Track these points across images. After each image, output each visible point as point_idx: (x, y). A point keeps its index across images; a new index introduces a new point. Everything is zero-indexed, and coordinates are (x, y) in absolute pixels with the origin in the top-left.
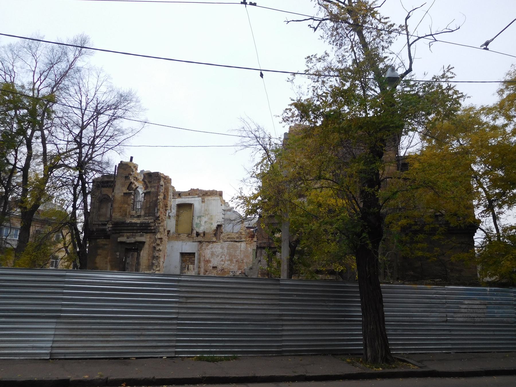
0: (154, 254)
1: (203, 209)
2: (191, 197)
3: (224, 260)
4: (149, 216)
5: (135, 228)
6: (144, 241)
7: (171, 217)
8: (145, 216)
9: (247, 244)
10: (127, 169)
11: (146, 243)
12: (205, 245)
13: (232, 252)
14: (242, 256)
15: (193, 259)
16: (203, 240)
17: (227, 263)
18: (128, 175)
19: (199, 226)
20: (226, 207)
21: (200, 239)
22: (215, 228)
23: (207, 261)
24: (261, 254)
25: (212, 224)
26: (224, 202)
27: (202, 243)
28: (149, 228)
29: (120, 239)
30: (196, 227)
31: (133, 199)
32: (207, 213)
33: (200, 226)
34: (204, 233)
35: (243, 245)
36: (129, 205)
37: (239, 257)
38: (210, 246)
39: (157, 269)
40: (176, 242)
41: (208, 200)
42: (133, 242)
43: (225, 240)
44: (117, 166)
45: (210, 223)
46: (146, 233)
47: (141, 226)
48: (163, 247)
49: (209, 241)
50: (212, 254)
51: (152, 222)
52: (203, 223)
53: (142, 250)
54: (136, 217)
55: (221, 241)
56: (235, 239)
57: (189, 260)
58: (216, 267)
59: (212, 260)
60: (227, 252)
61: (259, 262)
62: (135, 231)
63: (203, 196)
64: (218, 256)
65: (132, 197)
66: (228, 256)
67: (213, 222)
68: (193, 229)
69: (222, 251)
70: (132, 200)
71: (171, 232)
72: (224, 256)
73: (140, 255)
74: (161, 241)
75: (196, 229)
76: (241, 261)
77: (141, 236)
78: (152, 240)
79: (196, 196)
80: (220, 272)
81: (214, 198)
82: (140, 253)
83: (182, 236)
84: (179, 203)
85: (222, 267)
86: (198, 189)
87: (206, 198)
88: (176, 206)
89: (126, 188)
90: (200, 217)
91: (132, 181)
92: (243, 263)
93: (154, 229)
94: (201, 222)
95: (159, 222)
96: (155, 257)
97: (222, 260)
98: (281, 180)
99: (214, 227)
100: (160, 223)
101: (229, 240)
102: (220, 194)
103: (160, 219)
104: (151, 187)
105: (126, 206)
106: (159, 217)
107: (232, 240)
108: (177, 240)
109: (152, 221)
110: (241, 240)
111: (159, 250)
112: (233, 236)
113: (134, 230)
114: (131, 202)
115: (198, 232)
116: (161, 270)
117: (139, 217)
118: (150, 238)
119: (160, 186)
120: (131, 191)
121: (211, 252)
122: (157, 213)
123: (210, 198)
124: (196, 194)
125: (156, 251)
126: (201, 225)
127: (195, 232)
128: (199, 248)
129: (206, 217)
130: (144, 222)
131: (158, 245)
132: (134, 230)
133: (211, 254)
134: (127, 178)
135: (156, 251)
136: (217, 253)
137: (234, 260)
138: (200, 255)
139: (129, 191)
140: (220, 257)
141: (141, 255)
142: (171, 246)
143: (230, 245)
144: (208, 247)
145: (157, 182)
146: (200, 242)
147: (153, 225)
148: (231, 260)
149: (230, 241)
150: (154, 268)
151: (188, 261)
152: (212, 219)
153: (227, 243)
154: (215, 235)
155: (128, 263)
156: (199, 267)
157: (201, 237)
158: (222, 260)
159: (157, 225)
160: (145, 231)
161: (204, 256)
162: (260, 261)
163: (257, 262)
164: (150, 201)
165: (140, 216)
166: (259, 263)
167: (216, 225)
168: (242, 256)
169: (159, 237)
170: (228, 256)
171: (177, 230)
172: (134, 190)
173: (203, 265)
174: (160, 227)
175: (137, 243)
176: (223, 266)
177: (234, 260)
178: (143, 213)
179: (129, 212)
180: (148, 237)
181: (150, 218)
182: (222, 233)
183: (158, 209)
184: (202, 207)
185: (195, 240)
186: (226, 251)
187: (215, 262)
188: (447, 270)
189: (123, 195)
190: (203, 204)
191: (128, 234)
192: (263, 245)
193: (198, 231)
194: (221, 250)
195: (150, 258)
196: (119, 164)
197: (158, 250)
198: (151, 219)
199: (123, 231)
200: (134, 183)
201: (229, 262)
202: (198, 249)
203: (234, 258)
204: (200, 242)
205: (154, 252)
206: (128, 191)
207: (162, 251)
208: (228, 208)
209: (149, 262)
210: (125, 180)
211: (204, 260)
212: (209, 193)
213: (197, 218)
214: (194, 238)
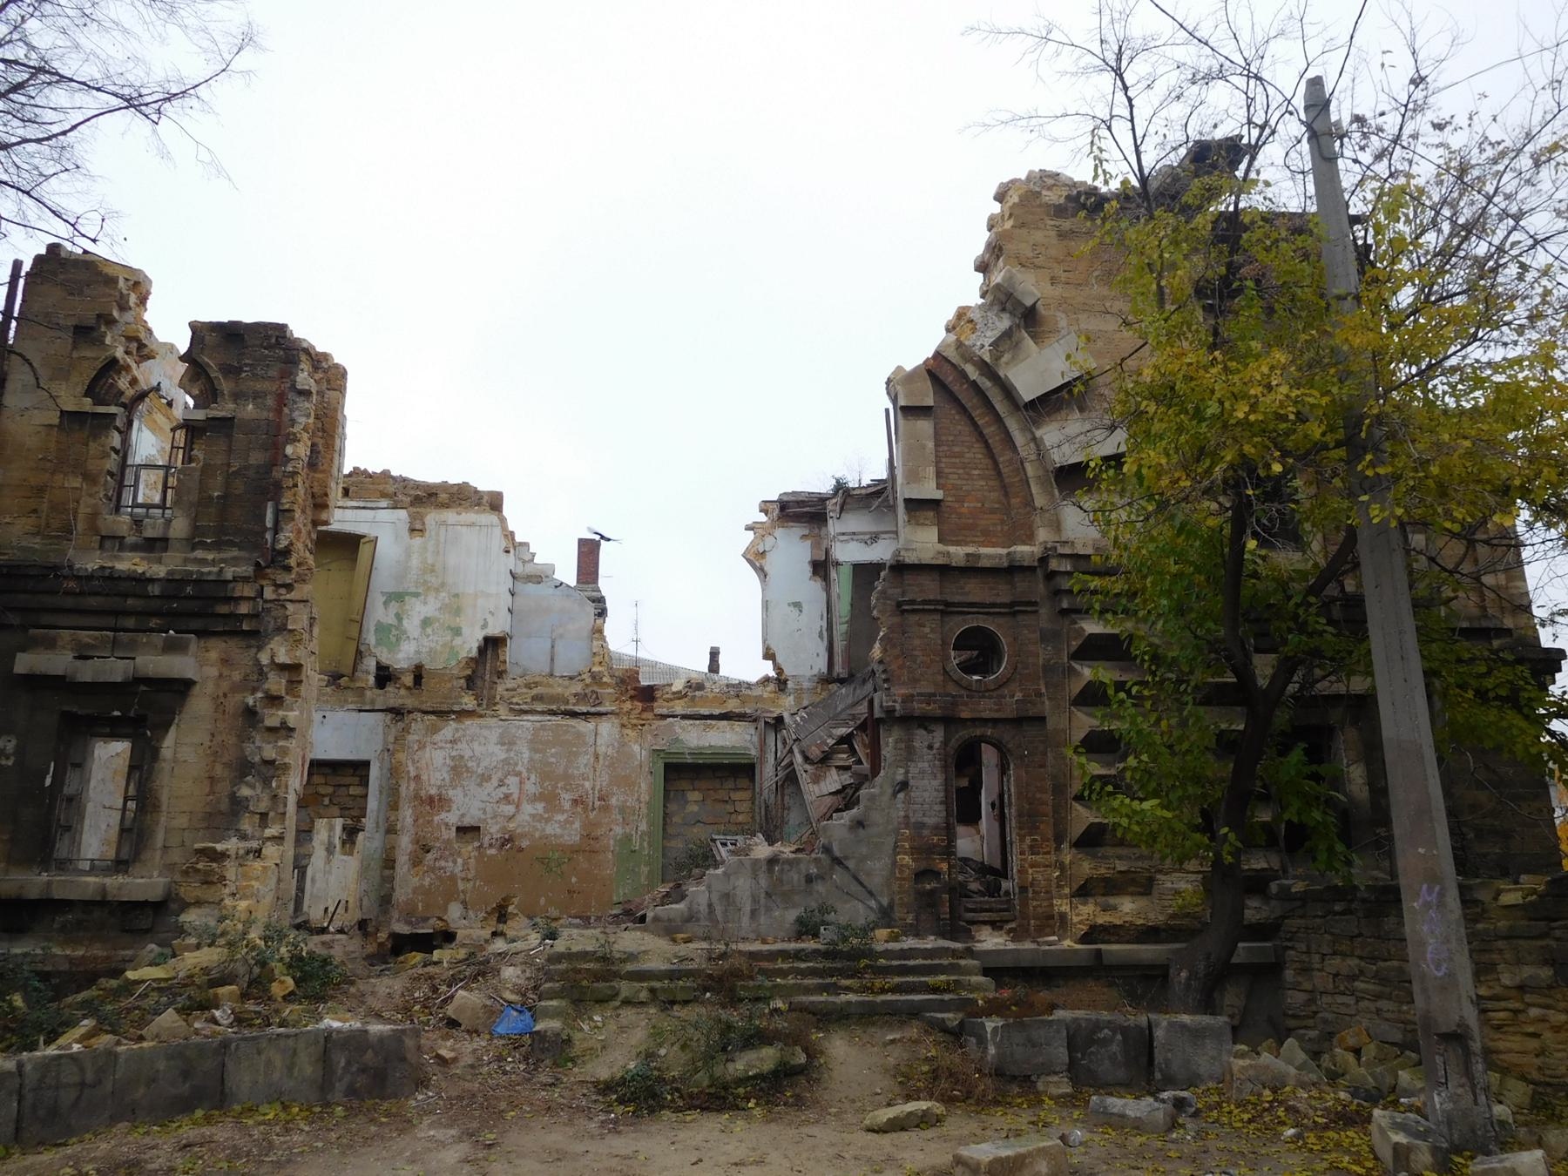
1: (415, 562)
3: (515, 796)
4: (218, 546)
5: (130, 601)
6: (190, 675)
8: (193, 542)
9: (623, 726)
10: (87, 291)
11: (197, 687)
12: (418, 725)
13: (553, 760)
14: (603, 779)
15: (353, 791)
16: (410, 702)
17: (528, 809)
18: (92, 322)
19: (393, 639)
20: (520, 564)
21: (394, 696)
22: (474, 653)
23: (431, 800)
24: (909, 754)
25: (457, 632)
26: (513, 546)
27: (408, 719)
28: (223, 609)
29: (25, 663)
30: (379, 642)
31: (117, 452)
32: (434, 581)
34: (419, 674)
35: (607, 729)
36: (91, 479)
37: (587, 785)
38: (449, 729)
39: (269, 832)
41: (444, 523)
42: (119, 680)
43: (524, 707)
44: (26, 267)
45: (449, 628)
46: (202, 634)
47: (175, 597)
49: (444, 708)
50: (458, 769)
51: (245, 579)
52: (412, 625)
53: (173, 729)
54: (135, 548)
55: (502, 710)
56: (567, 703)
57: (331, 796)
58: (476, 829)
59: (455, 794)
60: (531, 760)
61: (895, 794)
62: (130, 622)
63: (412, 504)
64: (485, 778)
66: (533, 777)
67: (462, 622)
69: (503, 756)
70: (114, 455)
72: (517, 779)
73: (155, 754)
74: (290, 682)
75: (377, 651)
76: (597, 803)
77: (171, 647)
78: (237, 676)
79: (384, 503)
80: (493, 851)
81: (470, 516)
85: (504, 829)
86: (386, 474)
87: (432, 517)
89: (80, 389)
90: (398, 597)
91: (119, 353)
92: (606, 809)
93: (254, 616)
94: (405, 622)
95: (288, 578)
96: (253, 765)
97: (507, 798)
98: (1234, 336)
99: (467, 647)
101: (540, 707)
102: (494, 503)
103: (292, 562)
104: (237, 396)
105: (75, 482)
106: (287, 552)
107: (554, 707)
109: (246, 570)
110: (598, 709)
111: (285, 730)
112: (560, 690)
113: (117, 613)
114: (108, 467)
115: (387, 668)
117: (155, 546)
118: (225, 661)
119: (291, 395)
120: (113, 409)
121: (453, 758)
122: (276, 530)
123: (450, 516)
124: (384, 495)
126: (405, 632)
127: (370, 664)
128: (391, 739)
129: (431, 599)
130: (191, 573)
131: (274, 700)
132: (117, 613)
133: (454, 768)
134: (85, 333)
136: (483, 764)
137: (566, 797)
138: (394, 772)
139: (98, 402)
140: (495, 782)
143: (543, 728)
144: (437, 737)
145: (273, 373)
146: (397, 713)
147: (248, 591)
148: (549, 799)
149: (542, 713)
150: (246, 825)
151: (326, 801)
152: (458, 612)
153: (529, 722)
154: (471, 682)
155: (70, 799)
156: (391, 830)
157: (403, 692)
158: (507, 798)
159: (269, 593)
160: (196, 624)
161: (417, 778)
162: (904, 786)
163: (890, 791)
164: (229, 465)
165: (158, 544)
166: (901, 796)
167: (481, 638)
168: (603, 779)
169: (283, 657)
170: (533, 777)
172: (124, 405)
173: (409, 820)
174: (290, 606)
175: (143, 688)
176: (512, 826)
177: (566, 797)
178: (180, 528)
179: (94, 516)
180: (213, 655)
181: (223, 555)
182: (500, 674)
183: (278, 512)
184: (408, 555)
185: (373, 702)
186: (526, 755)
187: (468, 804)
188: (1464, 830)
189: (56, 421)
190: (418, 541)
191: (85, 636)
192: (919, 707)
193: (385, 658)
194: (500, 753)
195: (219, 770)
196: (38, 260)
197: (271, 730)
198: (235, 561)
199: (46, 619)
200: (127, 368)
201: (540, 807)
202: (385, 742)
203: (564, 788)
204: (397, 713)
205: (244, 737)
206: (87, 405)
208: (529, 569)
209: (212, 792)
210: (75, 347)
211: (417, 797)
212: (443, 496)
213: (386, 604)
214: (368, 693)
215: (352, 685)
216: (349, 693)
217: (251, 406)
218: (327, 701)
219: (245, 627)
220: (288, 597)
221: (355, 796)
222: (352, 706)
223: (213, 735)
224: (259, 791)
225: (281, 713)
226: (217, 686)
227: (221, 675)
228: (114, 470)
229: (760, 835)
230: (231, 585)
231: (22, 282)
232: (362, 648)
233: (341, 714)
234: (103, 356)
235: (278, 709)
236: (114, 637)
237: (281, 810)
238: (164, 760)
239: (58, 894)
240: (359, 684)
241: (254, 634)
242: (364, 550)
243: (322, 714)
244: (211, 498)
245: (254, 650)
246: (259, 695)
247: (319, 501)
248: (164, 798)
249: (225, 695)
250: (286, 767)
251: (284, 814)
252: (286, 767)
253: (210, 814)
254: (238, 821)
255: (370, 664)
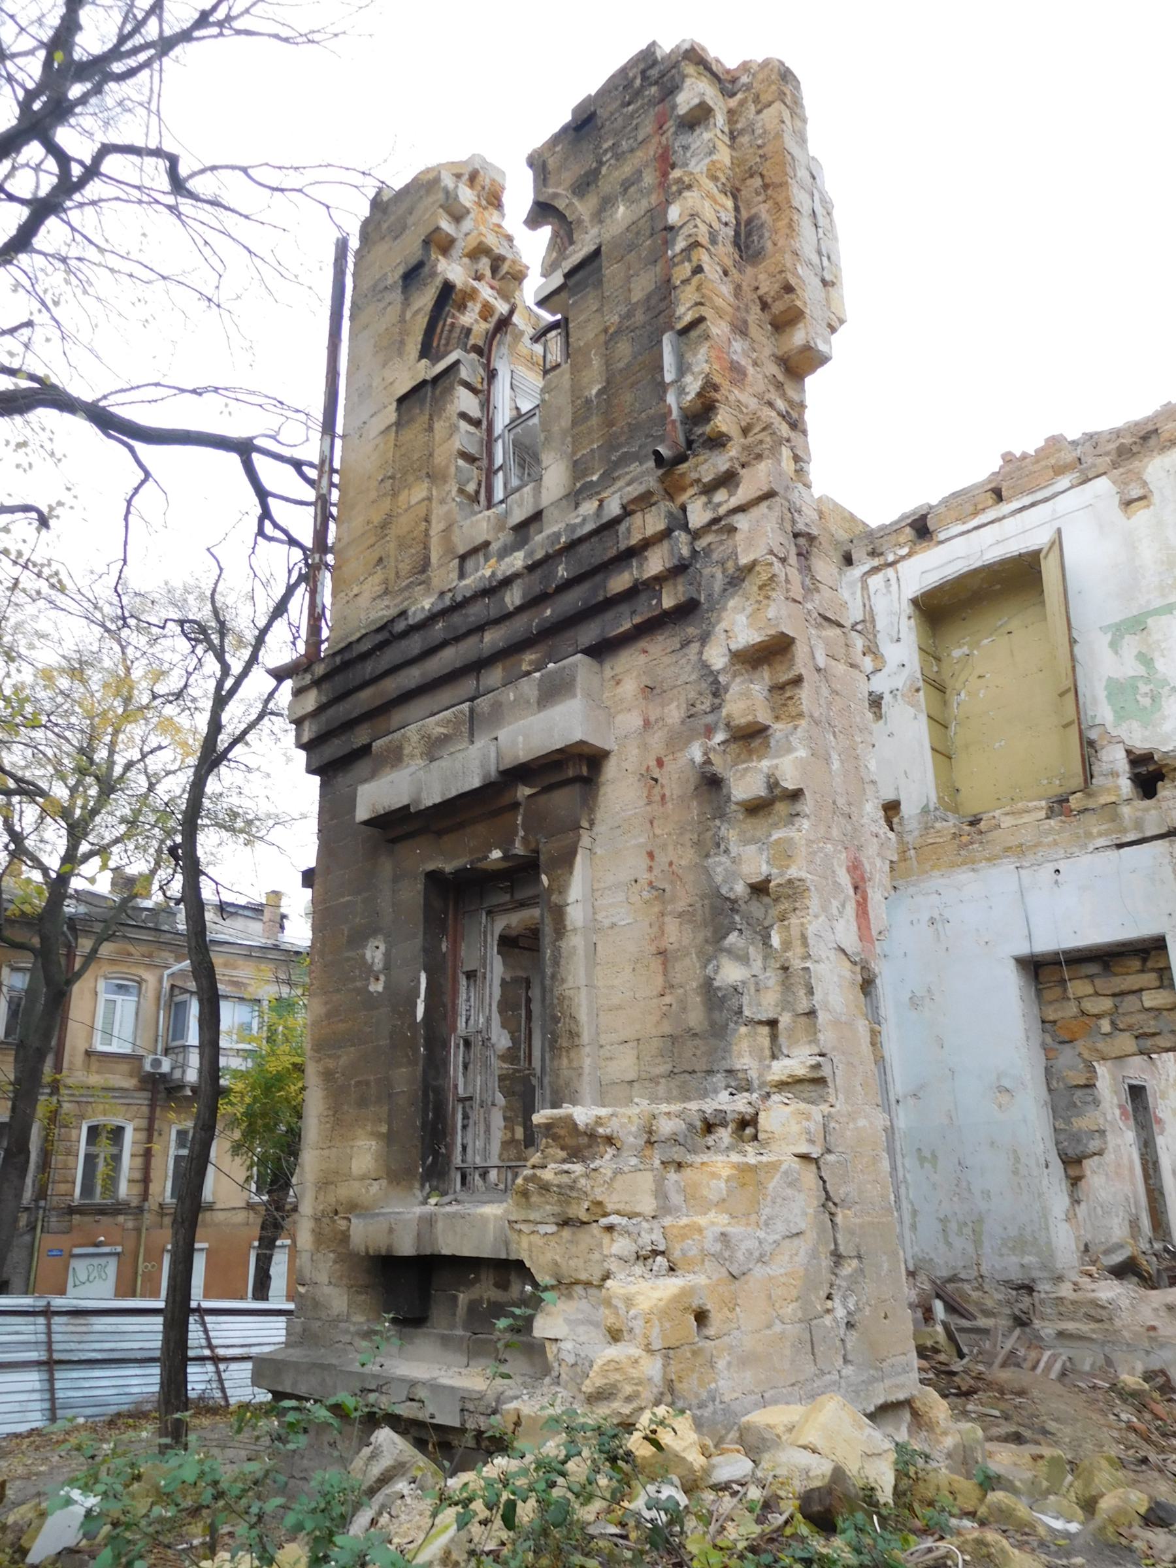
0: (719, 865)
1: (1148, 554)
2: (1016, 505)
7: (887, 698)
19: (1146, 702)
30: (1121, 715)
33: (1155, 698)
39: (780, 1069)
40: (963, 876)
42: (476, 783)
44: (354, 244)
46: (600, 651)
48: (820, 756)
51: (645, 500)
53: (579, 859)
57: (1113, 1015)
63: (1115, 465)
65: (466, 401)
68: (1091, 743)
71: (908, 809)
75: (1122, 732)
77: (553, 692)
78: (674, 713)
79: (1064, 482)
82: (562, 890)
83: (1007, 822)
84: (932, 580)
88: (908, 609)
93: (680, 569)
94: (1160, 664)
96: (732, 905)
100: (728, 480)
108: (970, 863)
116: (839, 1073)
124: (1059, 470)
125: (731, 834)
127: (1115, 759)
135: (731, 834)
141: (575, 915)
142: (925, 917)
147: (652, 522)
151: (1105, 1026)
159: (698, 515)
171: (950, 793)
190: (1142, 516)
191: (435, 725)
193: (1141, 742)
195: (675, 934)
207: (807, 805)
213: (1114, 645)
214: (1126, 810)
215: (1091, 804)
216: (1090, 818)
217: (622, 209)
218: (1055, 843)
219: (668, 602)
220: (734, 502)
221: (1158, 1010)
222: (1101, 842)
223: (651, 855)
224: (757, 965)
225: (765, 764)
226: (645, 747)
227: (647, 724)
228: (472, 450)
229: (192, 1395)
230: (622, 528)
231: (351, 259)
232: (1093, 735)
233: (1086, 861)
234: (438, 282)
235: (760, 759)
236: (472, 710)
237: (803, 1005)
238: (575, 930)
239: (448, 1246)
240: (1104, 799)
241: (688, 610)
242: (1049, 569)
243: (1051, 867)
244: (588, 401)
245: (695, 647)
246: (720, 737)
247: (777, 307)
248: (583, 1016)
249: (660, 763)
250: (794, 891)
251: (811, 1013)
252: (794, 891)
253: (673, 1039)
254: (727, 1050)
255: (1115, 759)
